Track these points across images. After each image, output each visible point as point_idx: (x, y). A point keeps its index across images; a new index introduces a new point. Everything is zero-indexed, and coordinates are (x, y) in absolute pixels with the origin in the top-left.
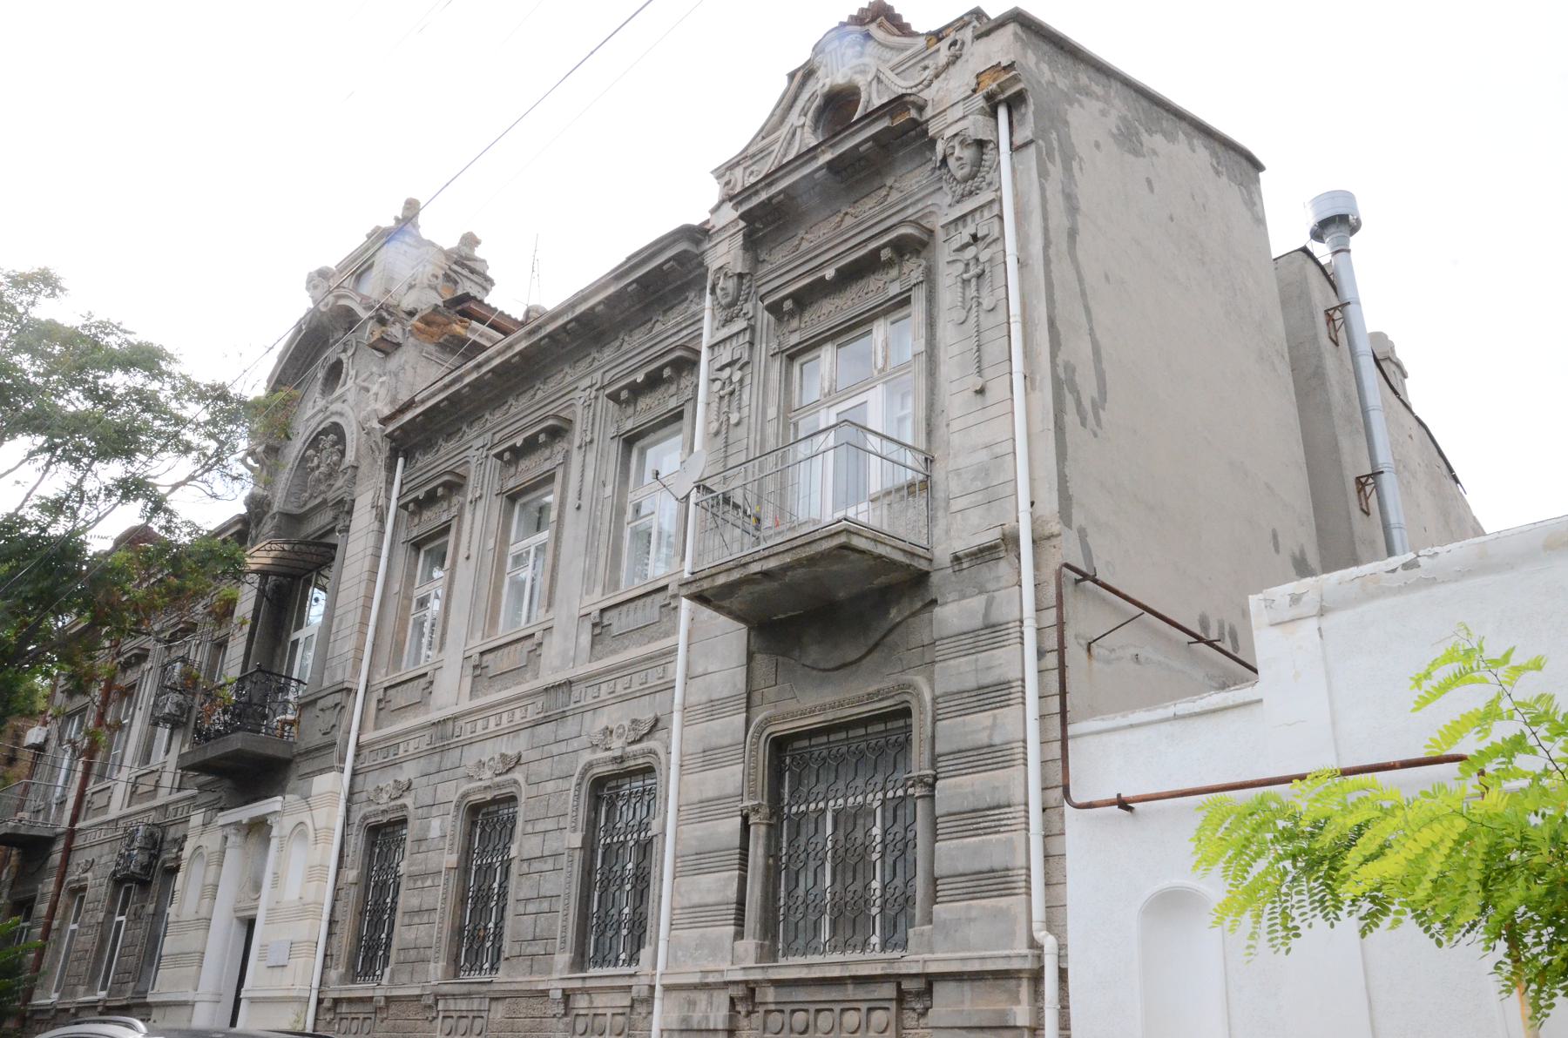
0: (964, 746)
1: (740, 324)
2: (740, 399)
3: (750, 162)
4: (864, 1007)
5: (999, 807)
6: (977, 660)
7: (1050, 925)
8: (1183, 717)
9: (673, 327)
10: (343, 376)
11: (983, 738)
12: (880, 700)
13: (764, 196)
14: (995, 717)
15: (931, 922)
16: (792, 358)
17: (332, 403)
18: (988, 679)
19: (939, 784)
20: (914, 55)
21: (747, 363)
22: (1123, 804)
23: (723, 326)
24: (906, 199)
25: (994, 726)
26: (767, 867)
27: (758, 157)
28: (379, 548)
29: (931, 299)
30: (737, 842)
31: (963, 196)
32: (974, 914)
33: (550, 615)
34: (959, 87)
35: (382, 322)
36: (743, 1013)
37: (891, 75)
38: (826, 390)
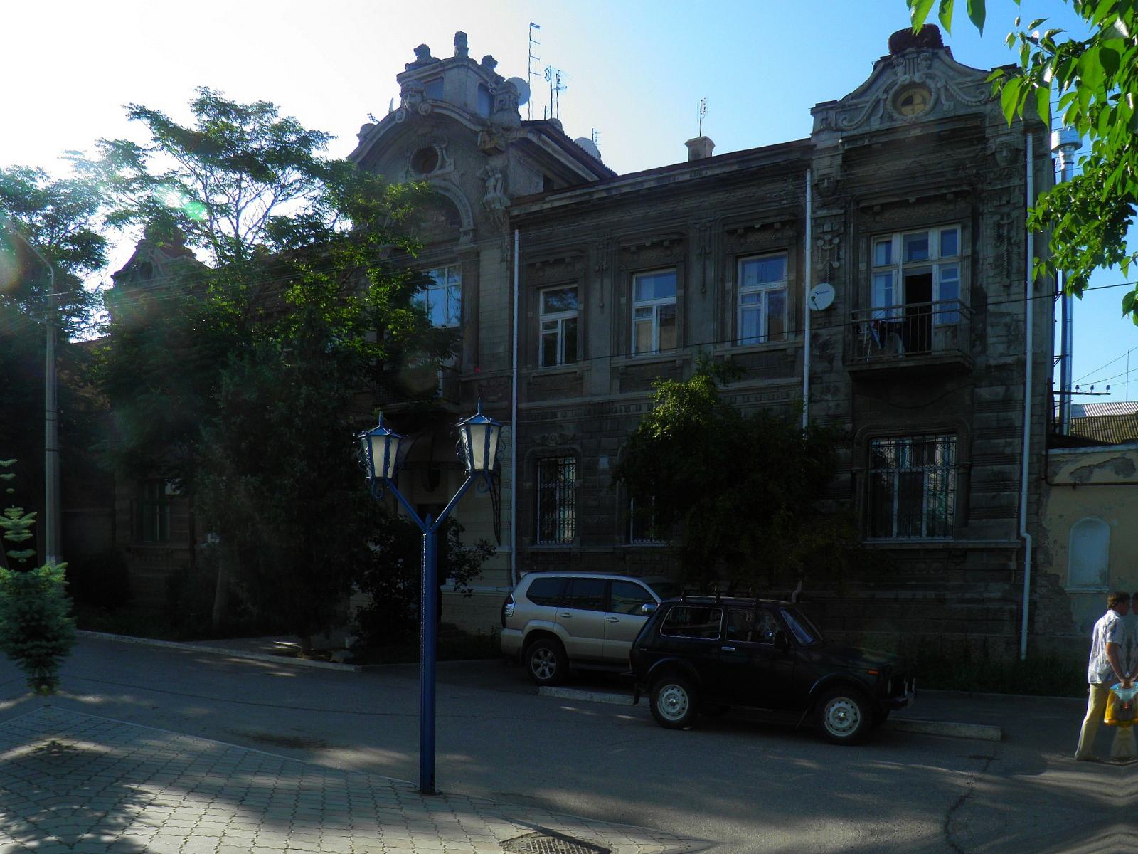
10: (439, 162)
23: (822, 207)
35: (490, 134)
37: (955, 88)
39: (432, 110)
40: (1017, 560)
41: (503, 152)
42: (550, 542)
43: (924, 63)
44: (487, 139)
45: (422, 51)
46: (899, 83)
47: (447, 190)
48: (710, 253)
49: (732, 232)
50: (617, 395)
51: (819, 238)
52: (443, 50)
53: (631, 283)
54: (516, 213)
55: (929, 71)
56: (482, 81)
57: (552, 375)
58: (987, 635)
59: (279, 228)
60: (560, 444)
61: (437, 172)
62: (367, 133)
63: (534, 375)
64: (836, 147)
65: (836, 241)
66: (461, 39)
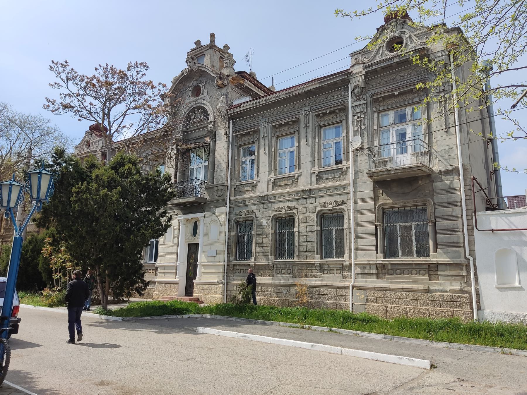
0: (444, 215)
1: (362, 102)
2: (364, 122)
3: (363, 54)
4: (418, 270)
5: (455, 229)
6: (447, 196)
7: (470, 255)
8: (506, 213)
9: (336, 98)
11: (450, 213)
12: (417, 202)
13: (374, 67)
14: (453, 209)
15: (437, 252)
16: (277, 138)
17: (198, 100)
18: (451, 200)
19: (436, 222)
20: (423, 33)
21: (365, 113)
22: (493, 230)
23: (356, 101)
24: (419, 74)
25: (453, 211)
26: (383, 238)
27: (366, 53)
28: (229, 146)
29: (299, 134)
30: (375, 232)
31: (357, 100)
32: (449, 251)
33: (300, 171)
34: (440, 47)
36: (380, 270)
37: (414, 37)
38: (392, 123)
39: (198, 68)
40: (466, 270)
41: (226, 86)
42: (242, 259)
43: (399, 27)
44: (219, 80)
45: (198, 43)
46: (389, 37)
47: (204, 104)
48: (309, 126)
49: (318, 116)
50: (271, 192)
51: (354, 116)
52: (206, 41)
53: (321, 132)
54: (230, 113)
55: (402, 30)
56: (221, 56)
57: (242, 184)
58: (454, 310)
59: (365, 72)
60: (247, 215)
61: (200, 96)
62: (174, 83)
63: (237, 184)
64: (361, 72)
65: (363, 116)
66: (213, 36)
